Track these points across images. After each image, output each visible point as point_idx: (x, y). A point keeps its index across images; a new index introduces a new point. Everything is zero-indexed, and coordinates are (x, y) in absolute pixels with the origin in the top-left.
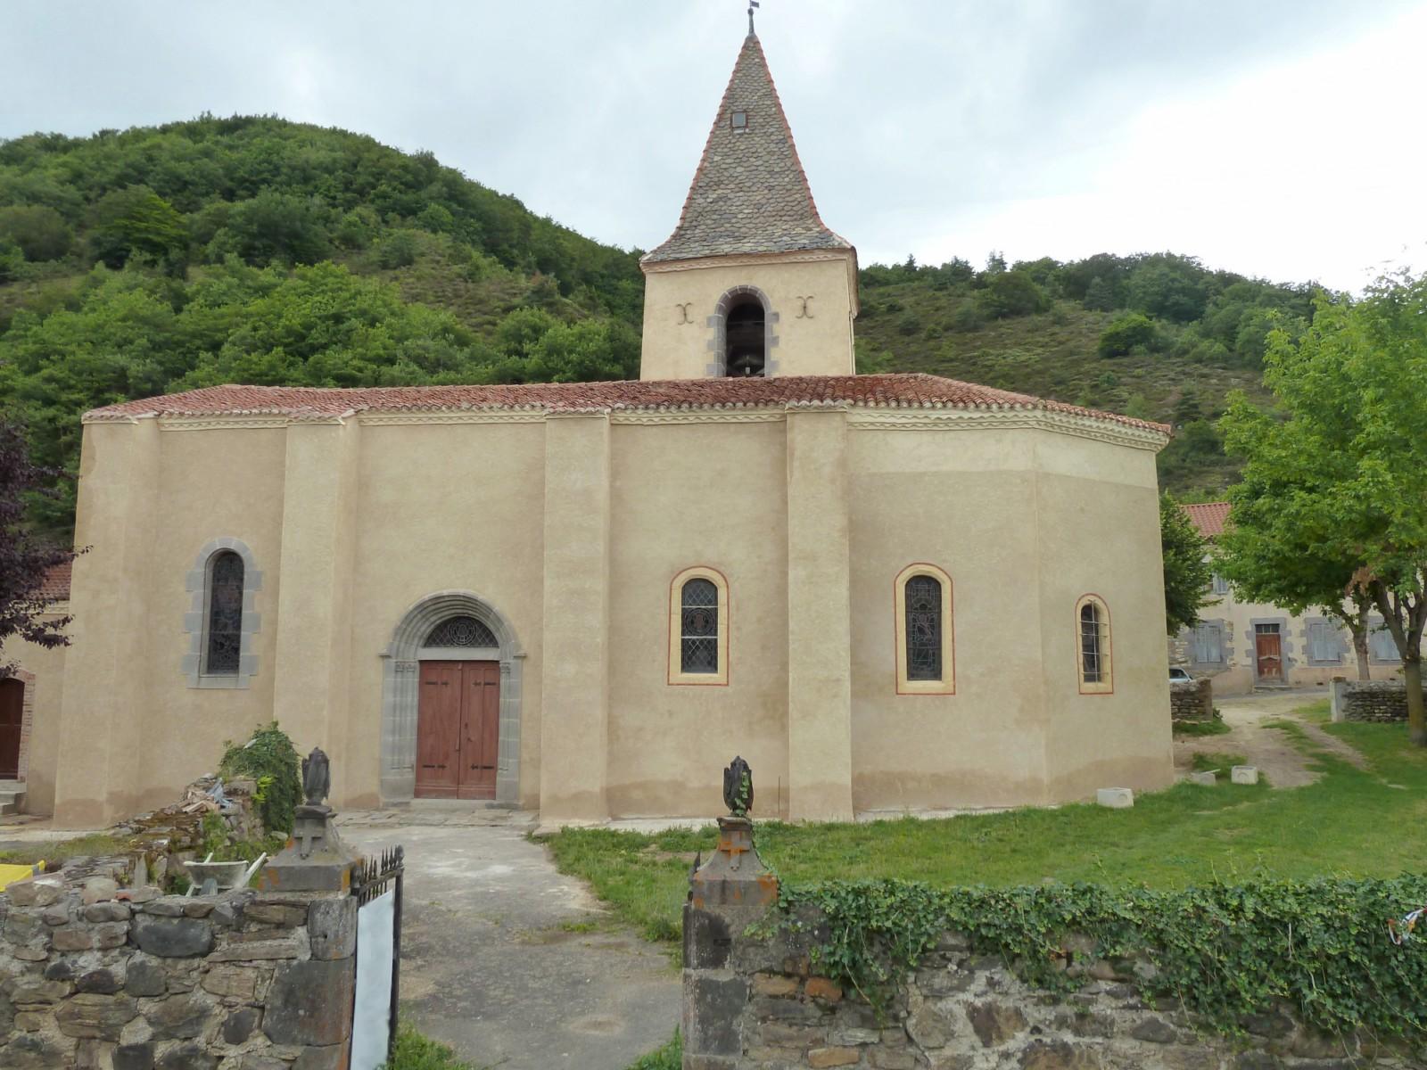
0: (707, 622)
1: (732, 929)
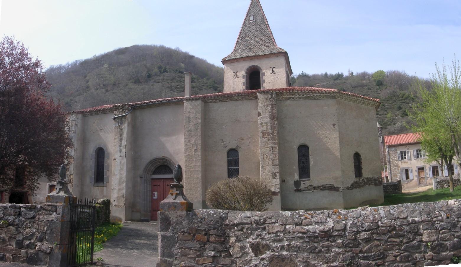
0: (236, 163)
1: (171, 219)
